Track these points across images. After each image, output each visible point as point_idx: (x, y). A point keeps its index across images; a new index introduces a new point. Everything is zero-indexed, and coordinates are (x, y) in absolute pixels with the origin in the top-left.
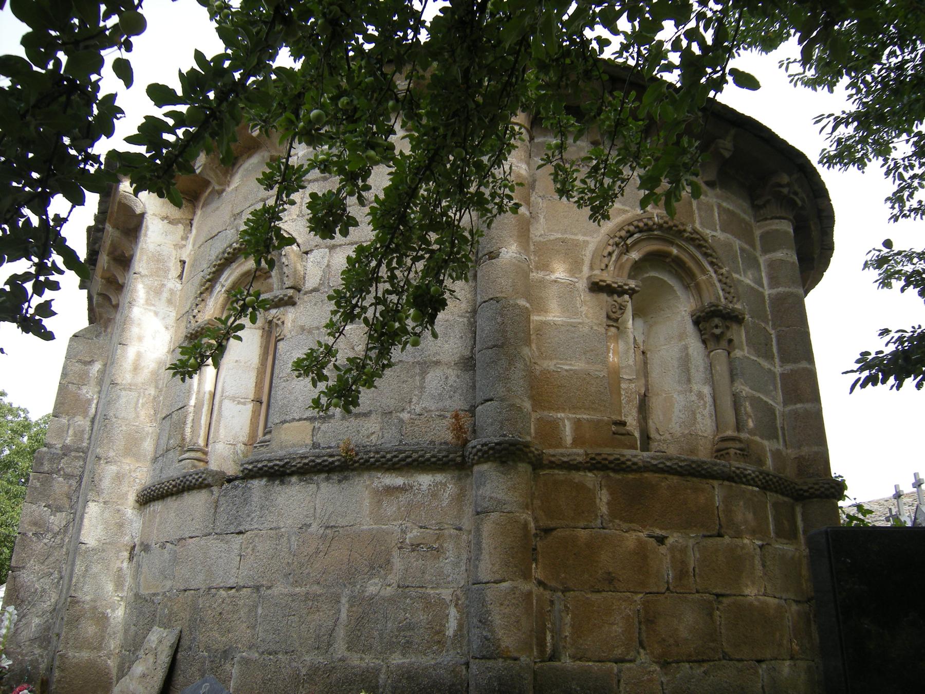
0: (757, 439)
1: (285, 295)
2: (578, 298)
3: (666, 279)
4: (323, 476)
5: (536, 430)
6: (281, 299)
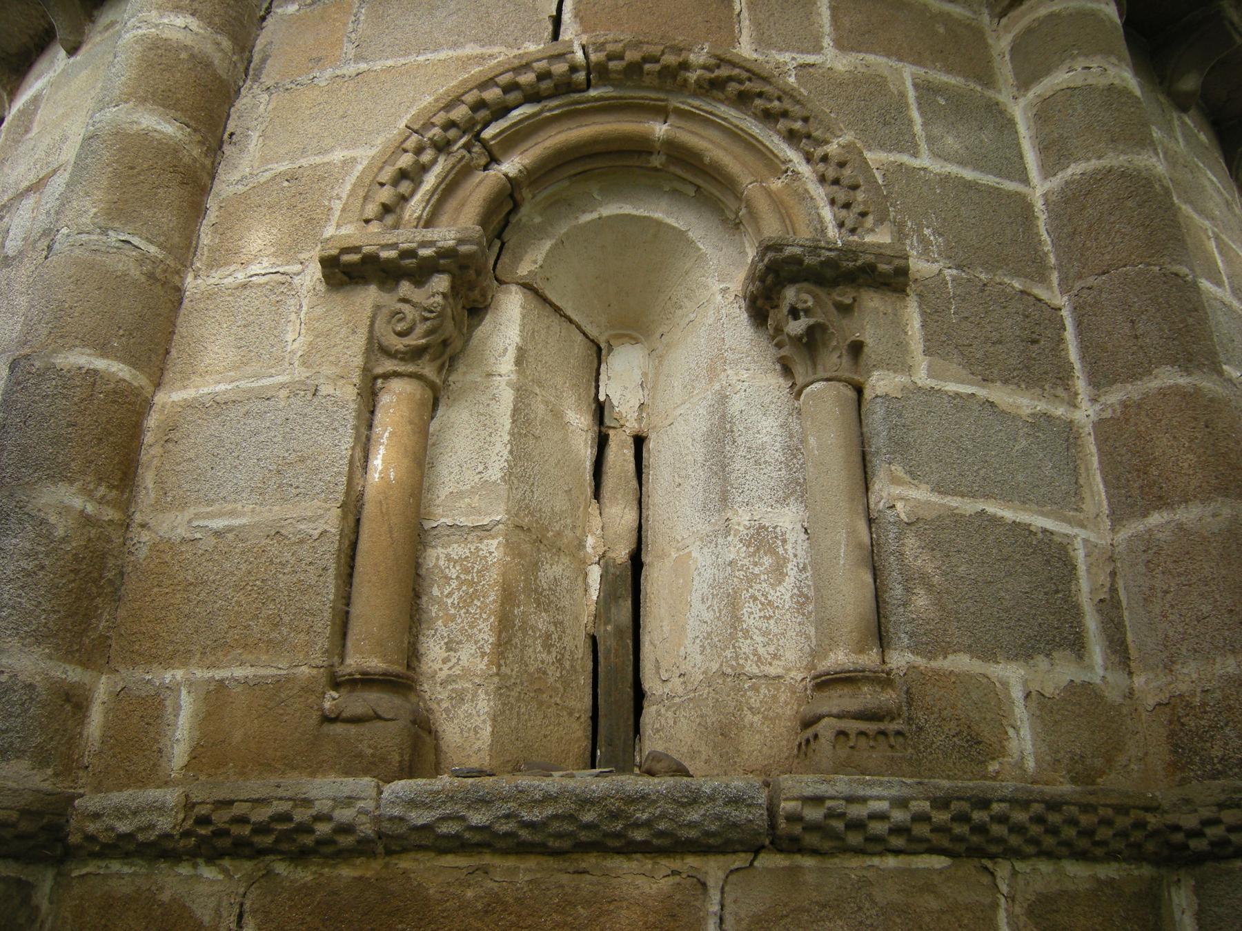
0: (961, 662)
2: (293, 317)
3: (658, 215)
5: (106, 727)
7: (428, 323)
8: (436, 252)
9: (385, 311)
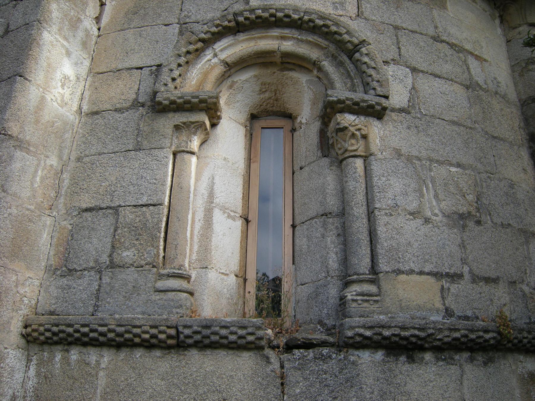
1: (377, 104)
4: (466, 355)
6: (372, 107)
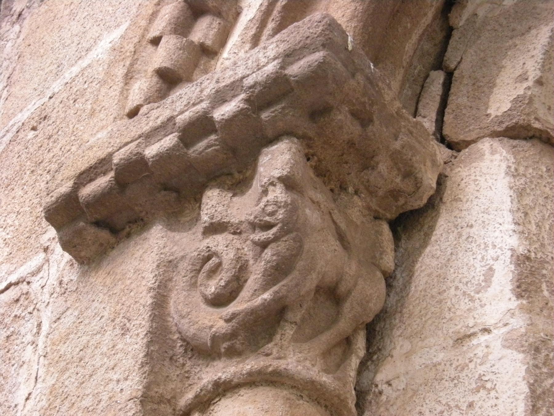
7: (268, 253)
8: (247, 101)
9: (184, 266)
